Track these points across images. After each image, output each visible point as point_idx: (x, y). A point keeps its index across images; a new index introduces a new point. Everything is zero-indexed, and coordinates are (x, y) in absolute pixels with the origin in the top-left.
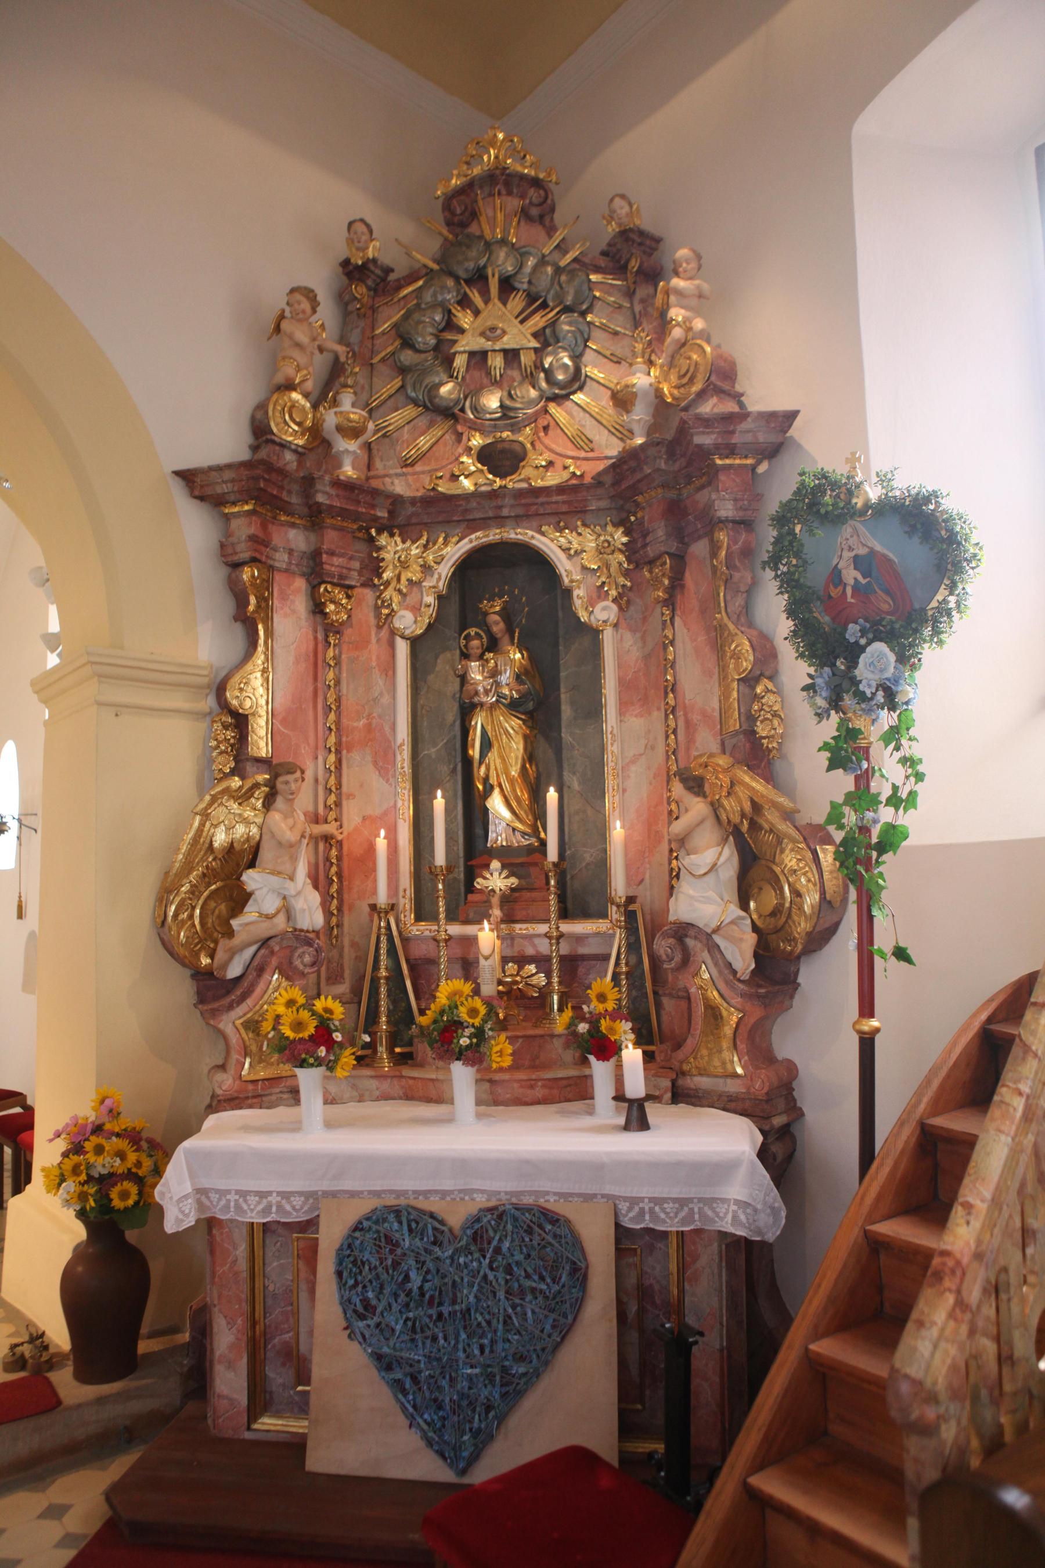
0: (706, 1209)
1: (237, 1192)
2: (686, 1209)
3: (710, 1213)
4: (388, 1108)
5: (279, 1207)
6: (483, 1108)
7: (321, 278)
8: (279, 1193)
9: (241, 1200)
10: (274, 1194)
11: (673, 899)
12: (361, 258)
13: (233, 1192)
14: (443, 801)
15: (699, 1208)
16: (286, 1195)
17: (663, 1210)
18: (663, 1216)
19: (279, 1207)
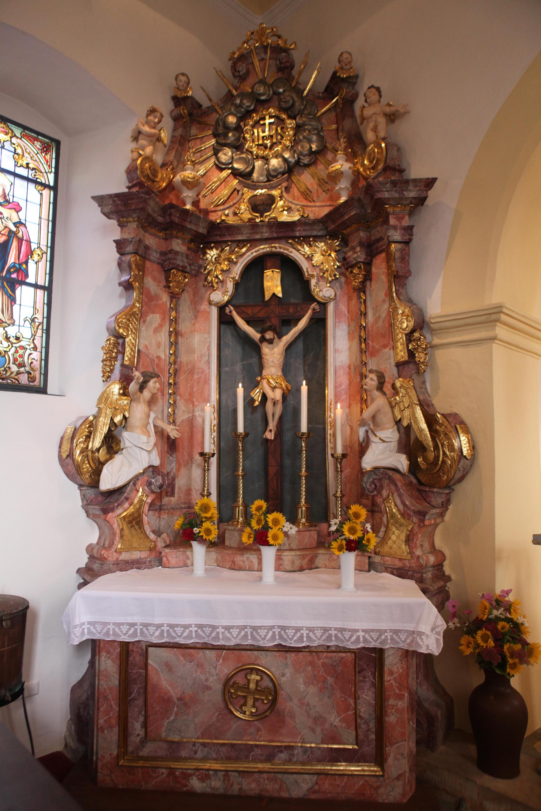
0: (311, 634)
1: (114, 624)
2: (188, 631)
3: (146, 631)
4: (297, 575)
5: (308, 636)
6: (357, 571)
7: (166, 106)
8: (391, 631)
9: (171, 630)
10: (111, 624)
11: (16, 308)
12: (254, 117)
13: (360, 631)
14: (307, 387)
15: (279, 632)
16: (311, 629)
17: (175, 631)
18: (258, 637)
19: (308, 636)
